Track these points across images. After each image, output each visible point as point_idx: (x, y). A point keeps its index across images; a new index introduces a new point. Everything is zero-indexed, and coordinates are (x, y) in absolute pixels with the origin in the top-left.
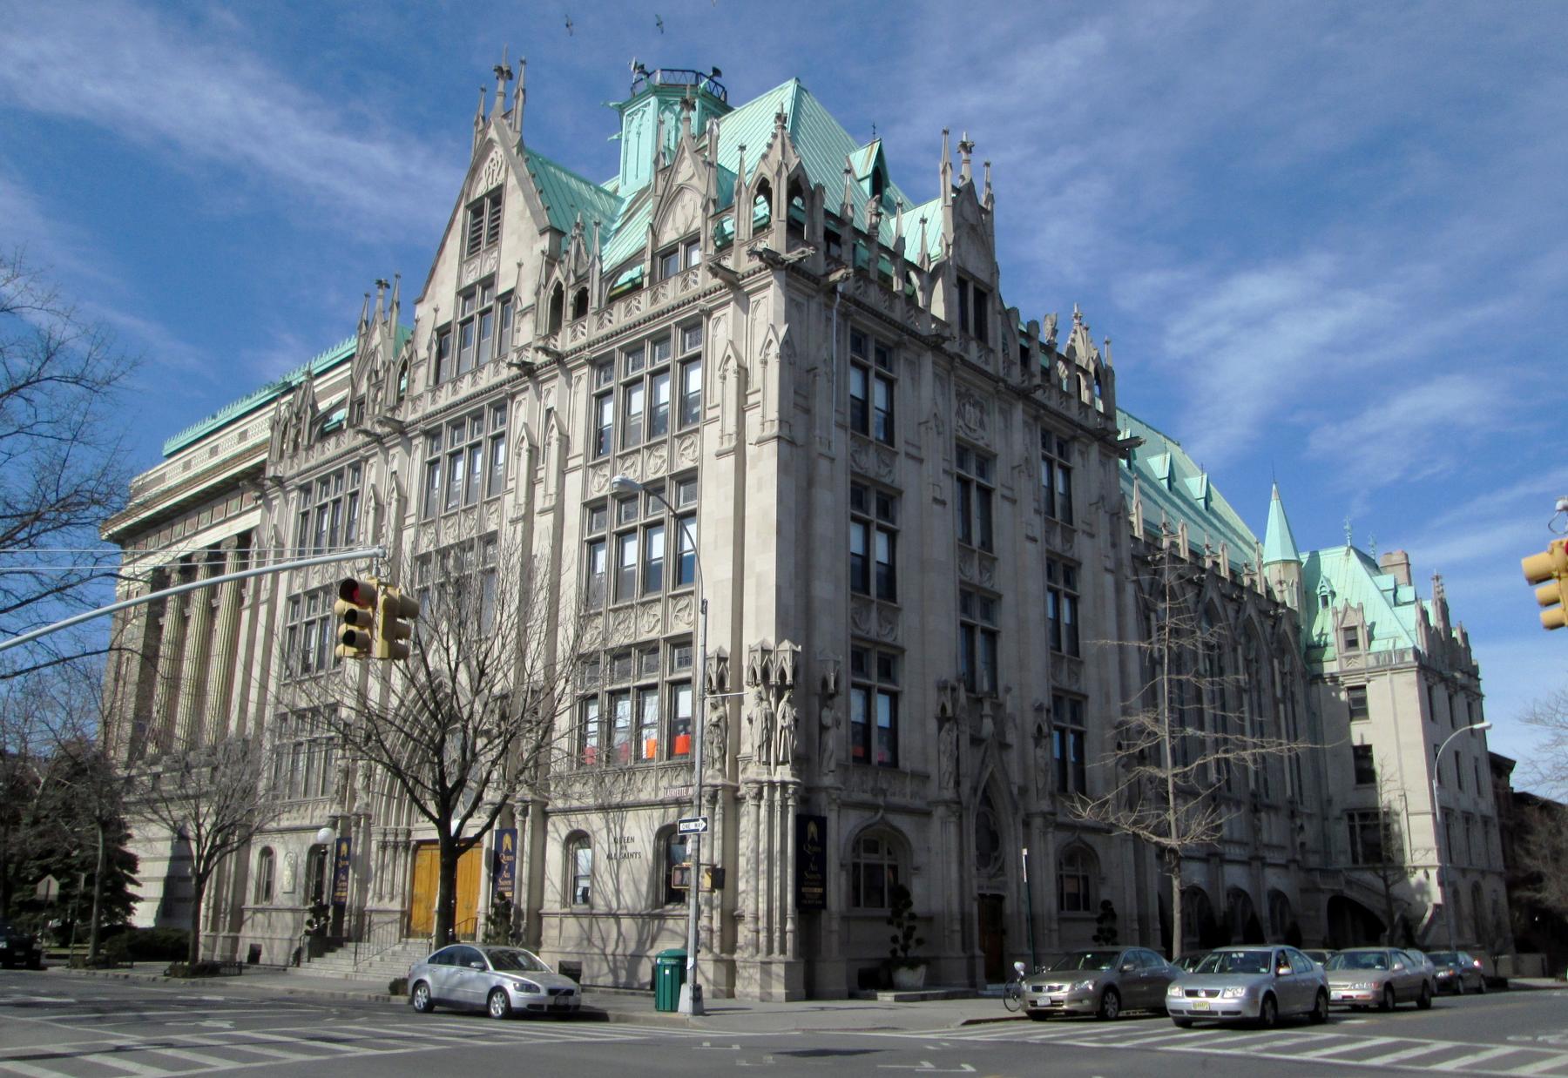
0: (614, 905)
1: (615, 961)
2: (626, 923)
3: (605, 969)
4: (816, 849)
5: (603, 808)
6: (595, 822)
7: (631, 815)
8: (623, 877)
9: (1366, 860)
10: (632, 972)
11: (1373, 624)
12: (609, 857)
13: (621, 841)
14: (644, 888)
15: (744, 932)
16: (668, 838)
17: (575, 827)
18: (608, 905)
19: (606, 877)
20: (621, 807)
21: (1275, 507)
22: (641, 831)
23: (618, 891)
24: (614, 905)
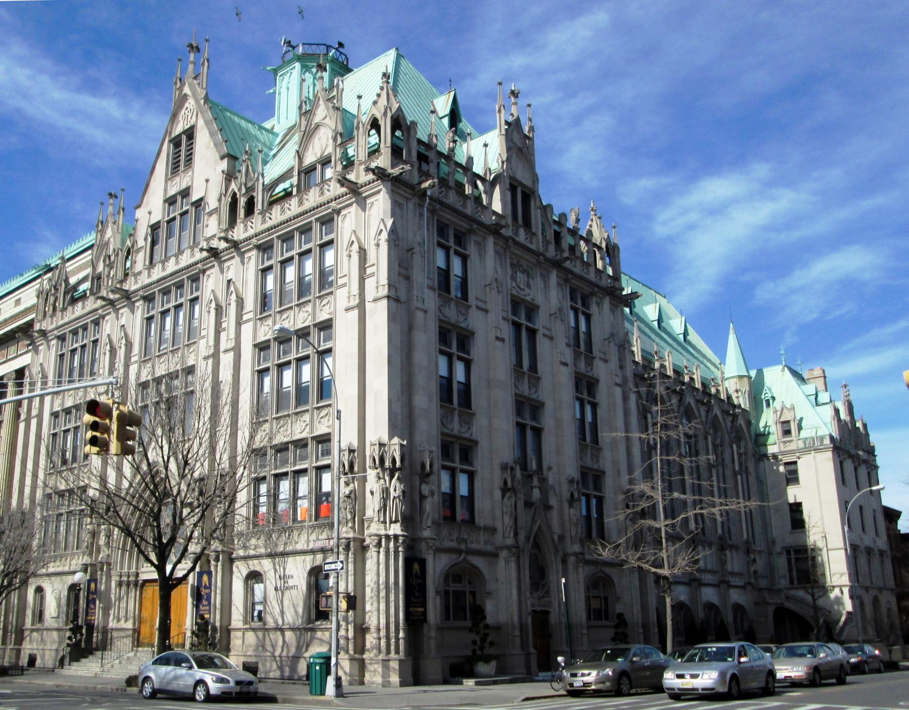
0: (280, 622)
1: (281, 661)
3: (275, 666)
5: (271, 556)
7: (290, 560)
8: (286, 603)
10: (294, 668)
12: (276, 589)
15: (370, 640)
16: (317, 575)
18: (276, 622)
20: (284, 554)
23: (282, 613)
24: (280, 622)
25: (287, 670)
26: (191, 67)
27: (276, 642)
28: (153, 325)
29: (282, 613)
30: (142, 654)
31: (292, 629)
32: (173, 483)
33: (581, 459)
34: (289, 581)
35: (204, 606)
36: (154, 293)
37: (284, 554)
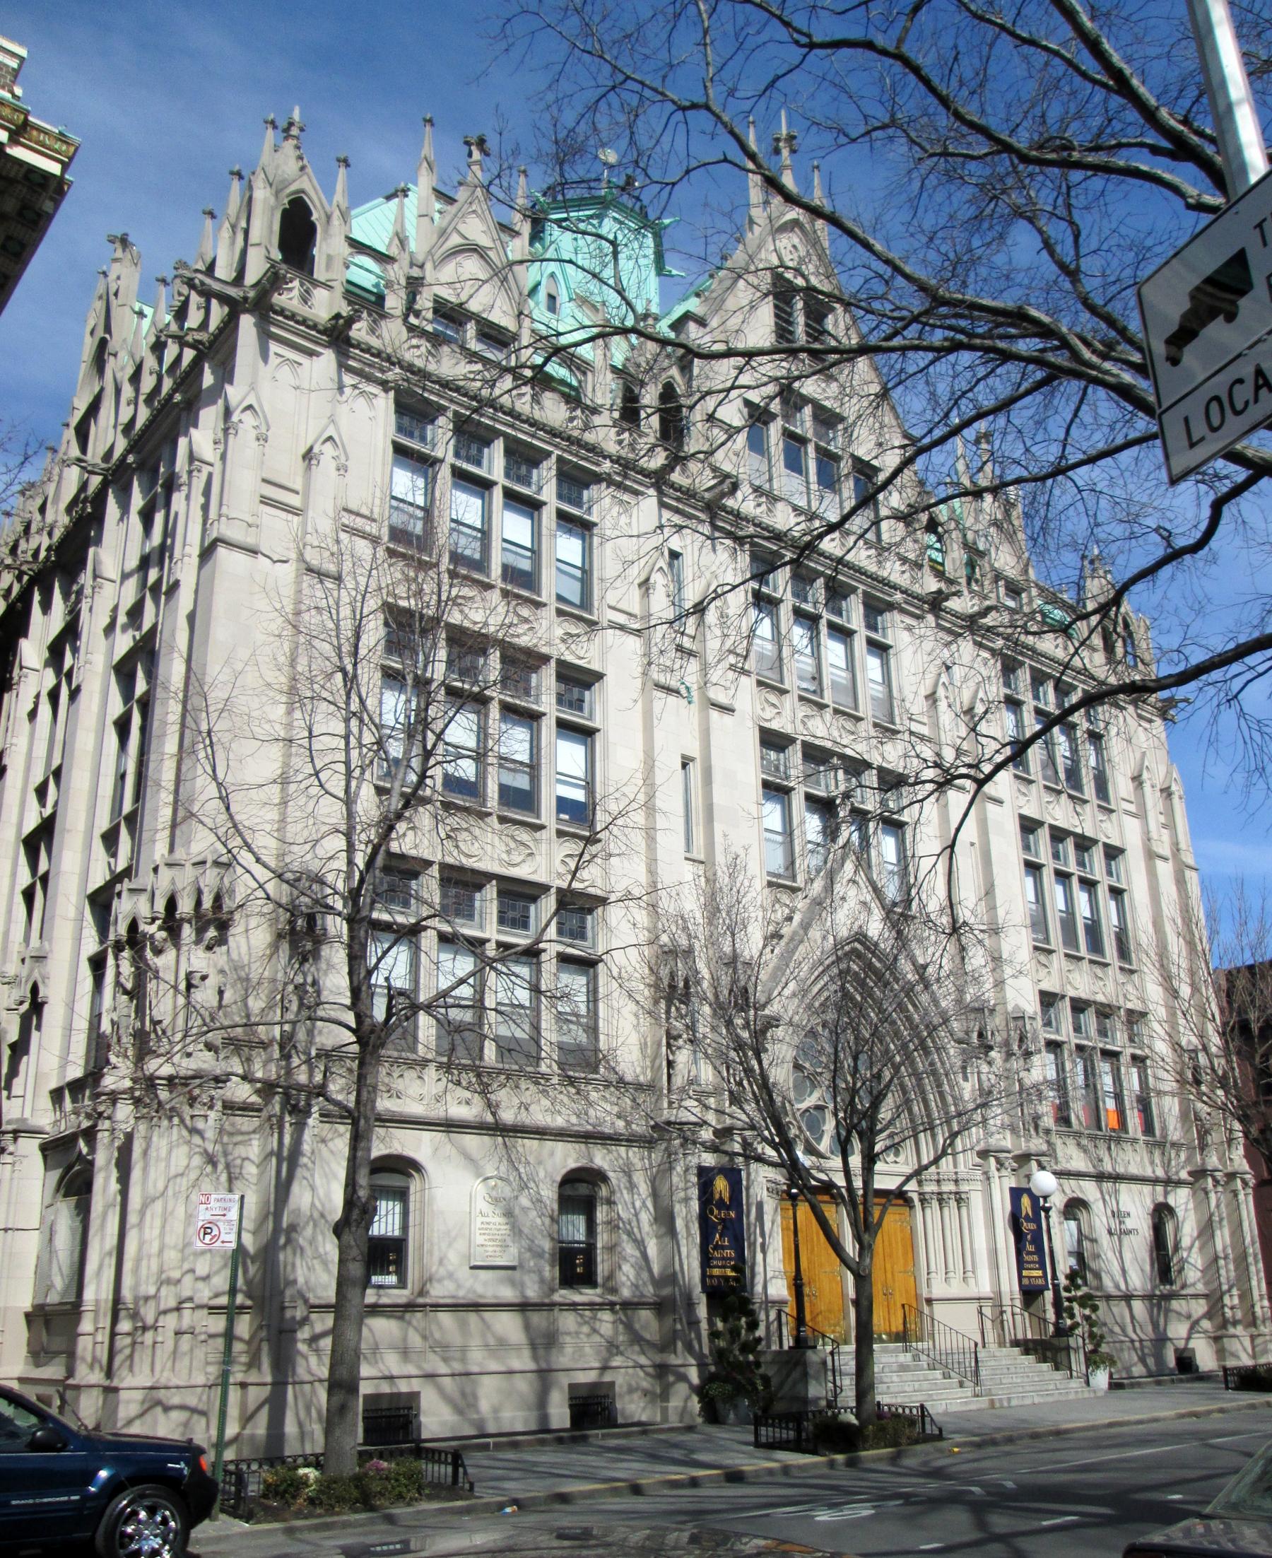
0: (1123, 1287)
1: (1142, 1347)
2: (1138, 1306)
3: (1136, 1359)
4: (1032, 1226)
5: (1100, 1177)
6: (1089, 1190)
7: (1123, 1187)
8: (1127, 1256)
9: (561, 1249)
10: (1159, 1358)
11: (769, 874)
12: (1110, 1233)
13: (1118, 1215)
14: (1147, 1268)
15: (238, 1347)
16: (1162, 1213)
17: (1071, 1195)
18: (1117, 1287)
19: (1110, 1254)
20: (1117, 1178)
21: (136, 484)
22: (1136, 1205)
23: (1124, 1271)
24: (1123, 1287)
25: (1151, 1361)
26: (1119, 644)
27: (1123, 1317)
28: (1115, 922)
29: (1124, 1271)
30: (134, 1380)
31: (1143, 1297)
32: (763, 976)
33: (1027, 847)
34: (1127, 1220)
35: (1029, 1253)
36: (549, 454)
37: (1117, 1178)
